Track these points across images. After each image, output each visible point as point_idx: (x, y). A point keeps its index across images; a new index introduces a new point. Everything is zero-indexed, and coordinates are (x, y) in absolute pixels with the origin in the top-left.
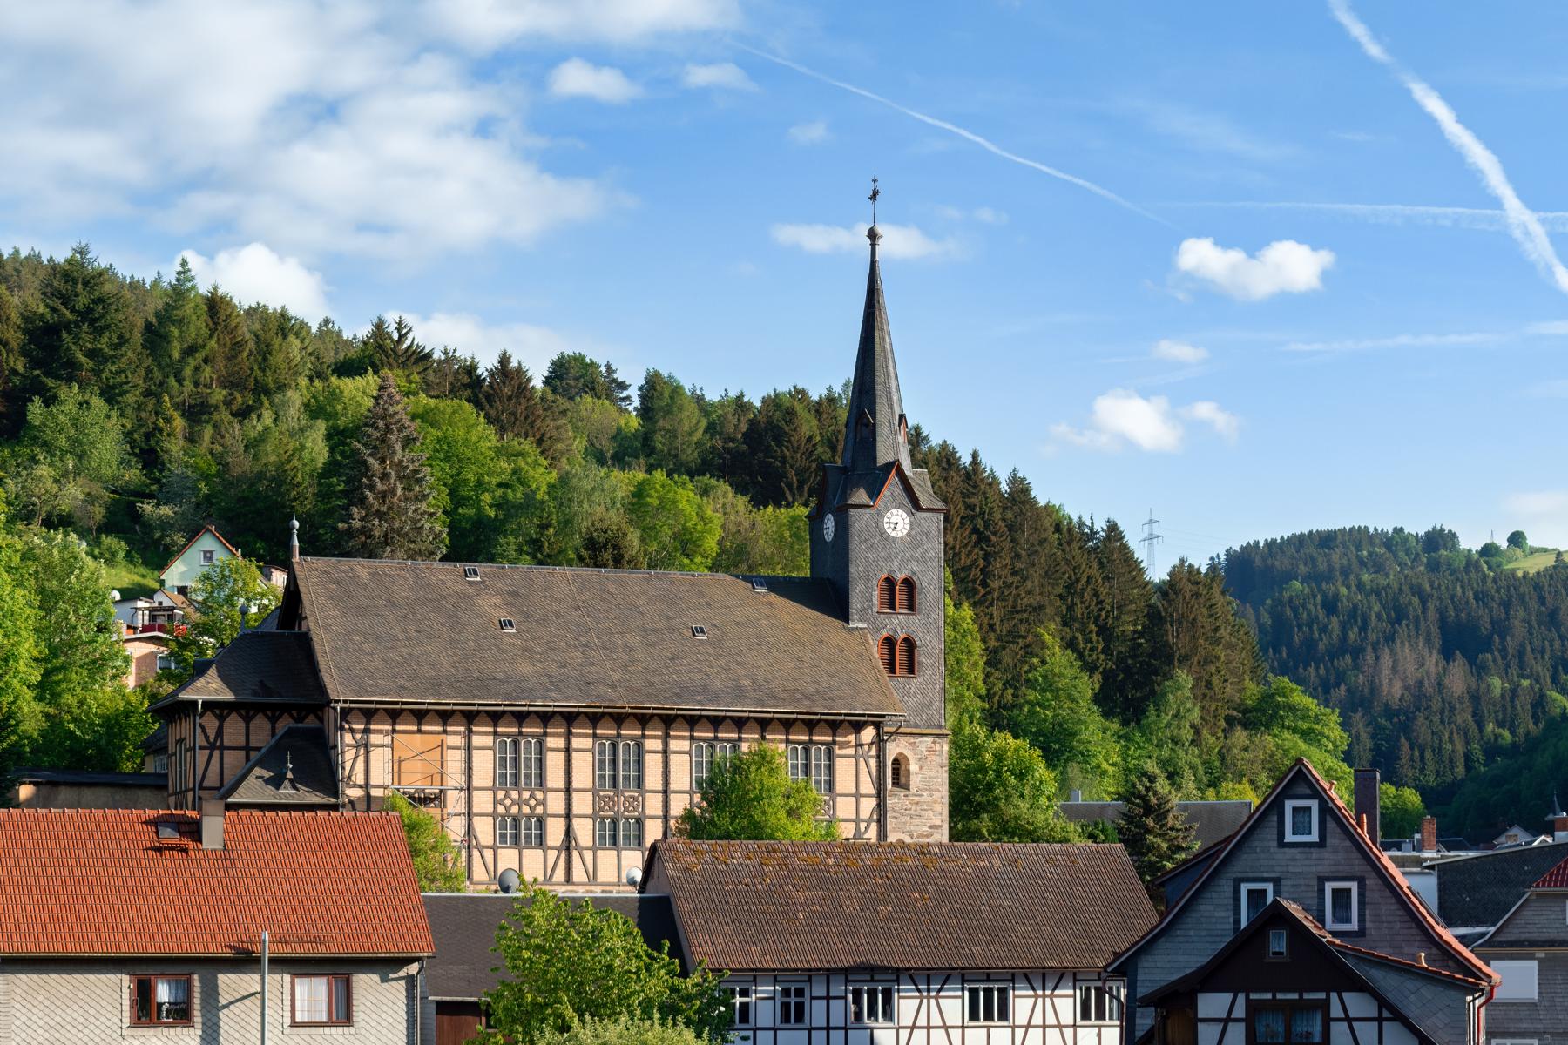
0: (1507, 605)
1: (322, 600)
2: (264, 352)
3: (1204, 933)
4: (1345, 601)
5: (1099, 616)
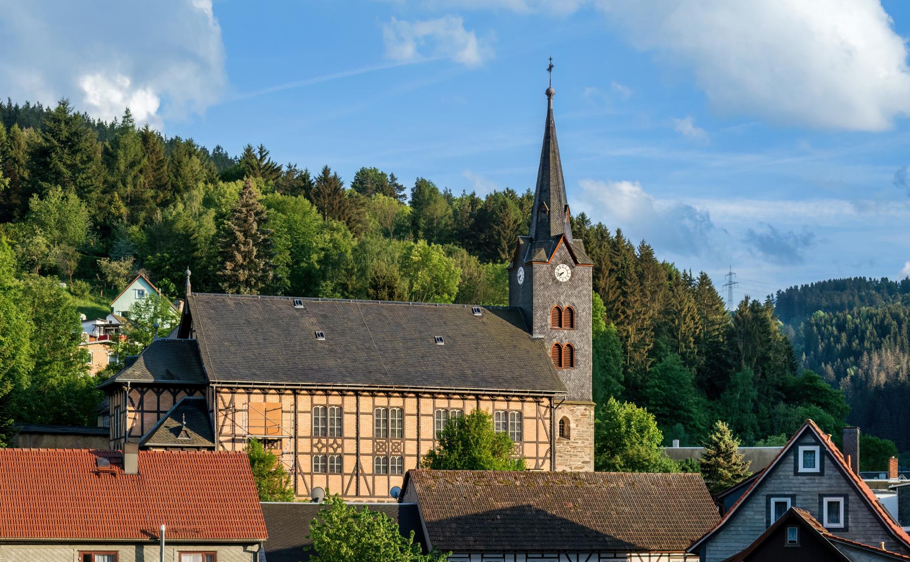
1: (205, 320)
2: (177, 167)
3: (748, 529)
4: (850, 323)
5: (695, 332)
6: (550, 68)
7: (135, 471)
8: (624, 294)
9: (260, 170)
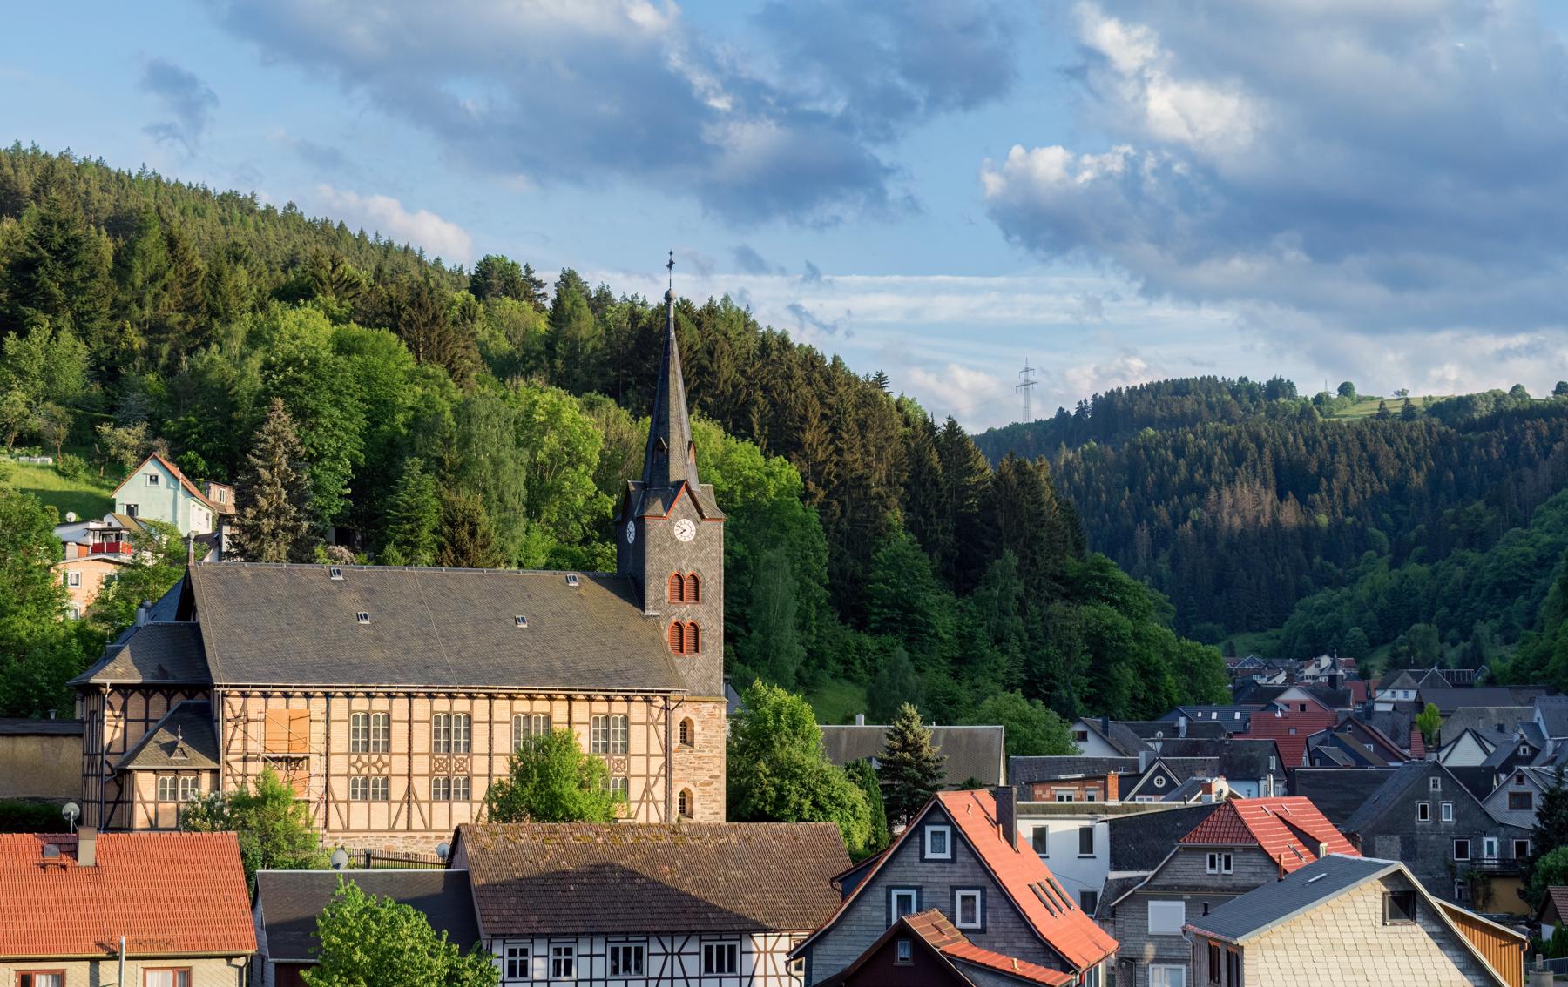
0: (1333, 449)
1: (211, 599)
7: (92, 863)
8: (839, 451)
9: (332, 284)
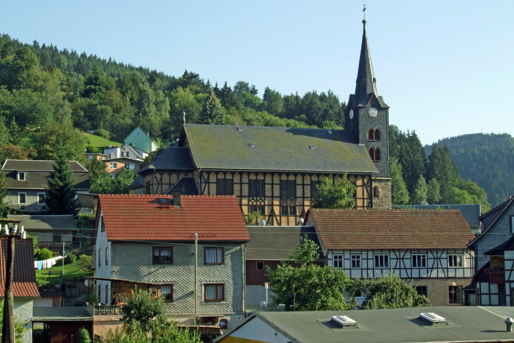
6: (364, 10)
